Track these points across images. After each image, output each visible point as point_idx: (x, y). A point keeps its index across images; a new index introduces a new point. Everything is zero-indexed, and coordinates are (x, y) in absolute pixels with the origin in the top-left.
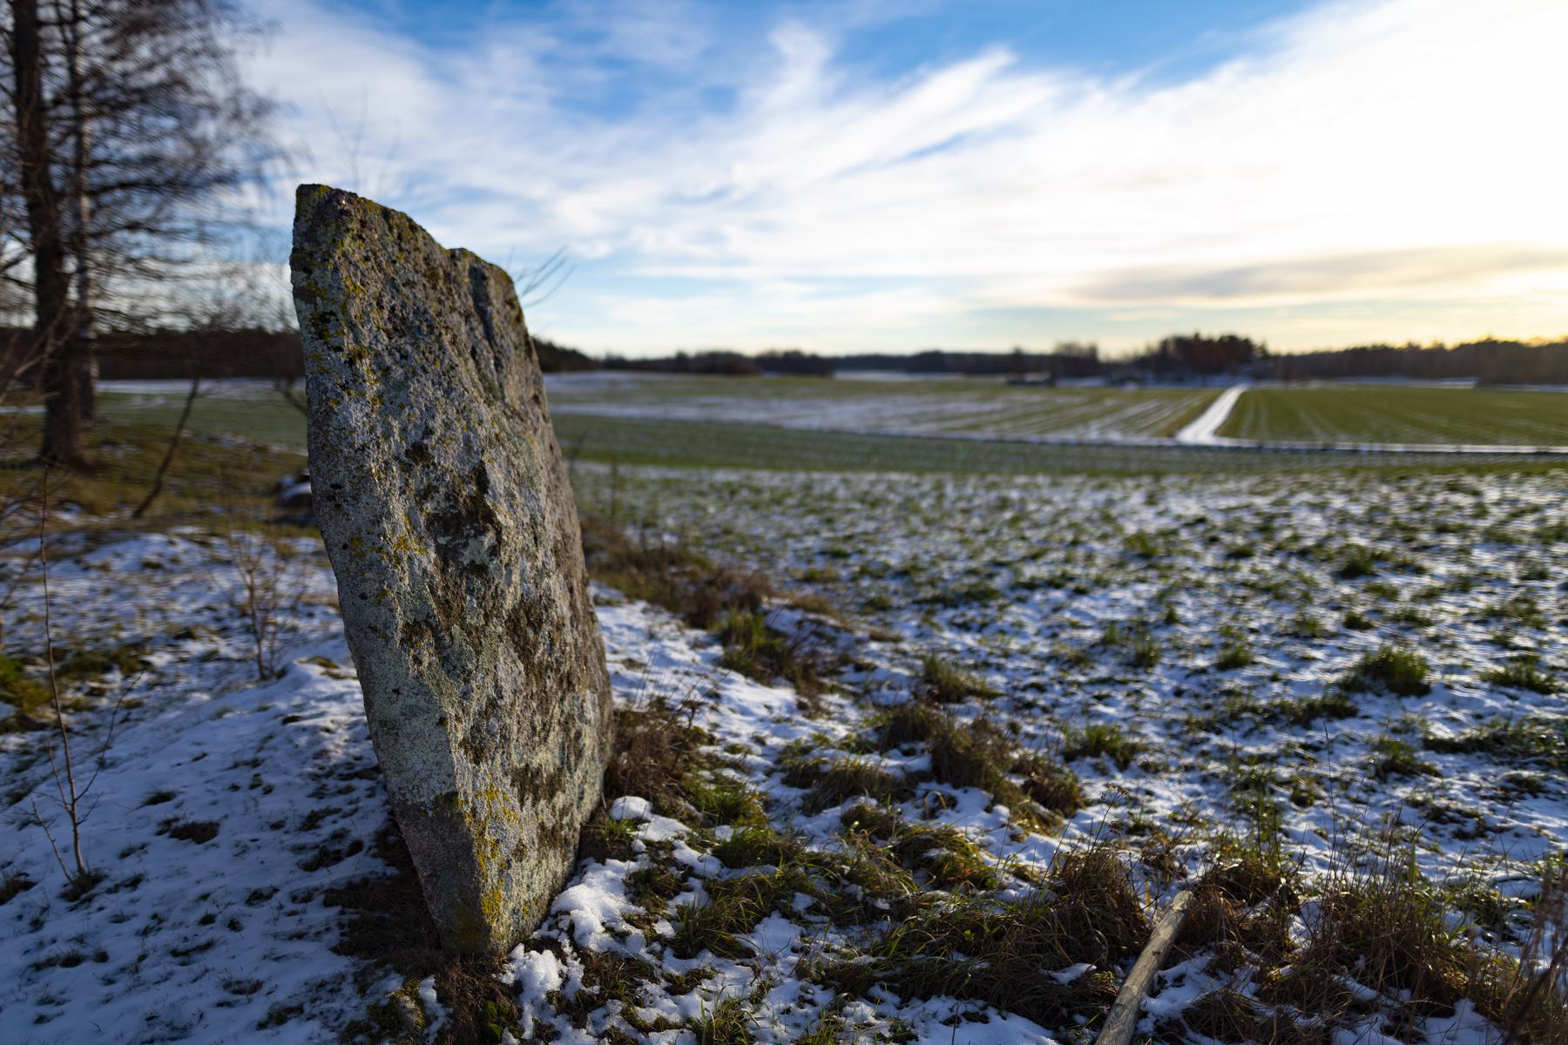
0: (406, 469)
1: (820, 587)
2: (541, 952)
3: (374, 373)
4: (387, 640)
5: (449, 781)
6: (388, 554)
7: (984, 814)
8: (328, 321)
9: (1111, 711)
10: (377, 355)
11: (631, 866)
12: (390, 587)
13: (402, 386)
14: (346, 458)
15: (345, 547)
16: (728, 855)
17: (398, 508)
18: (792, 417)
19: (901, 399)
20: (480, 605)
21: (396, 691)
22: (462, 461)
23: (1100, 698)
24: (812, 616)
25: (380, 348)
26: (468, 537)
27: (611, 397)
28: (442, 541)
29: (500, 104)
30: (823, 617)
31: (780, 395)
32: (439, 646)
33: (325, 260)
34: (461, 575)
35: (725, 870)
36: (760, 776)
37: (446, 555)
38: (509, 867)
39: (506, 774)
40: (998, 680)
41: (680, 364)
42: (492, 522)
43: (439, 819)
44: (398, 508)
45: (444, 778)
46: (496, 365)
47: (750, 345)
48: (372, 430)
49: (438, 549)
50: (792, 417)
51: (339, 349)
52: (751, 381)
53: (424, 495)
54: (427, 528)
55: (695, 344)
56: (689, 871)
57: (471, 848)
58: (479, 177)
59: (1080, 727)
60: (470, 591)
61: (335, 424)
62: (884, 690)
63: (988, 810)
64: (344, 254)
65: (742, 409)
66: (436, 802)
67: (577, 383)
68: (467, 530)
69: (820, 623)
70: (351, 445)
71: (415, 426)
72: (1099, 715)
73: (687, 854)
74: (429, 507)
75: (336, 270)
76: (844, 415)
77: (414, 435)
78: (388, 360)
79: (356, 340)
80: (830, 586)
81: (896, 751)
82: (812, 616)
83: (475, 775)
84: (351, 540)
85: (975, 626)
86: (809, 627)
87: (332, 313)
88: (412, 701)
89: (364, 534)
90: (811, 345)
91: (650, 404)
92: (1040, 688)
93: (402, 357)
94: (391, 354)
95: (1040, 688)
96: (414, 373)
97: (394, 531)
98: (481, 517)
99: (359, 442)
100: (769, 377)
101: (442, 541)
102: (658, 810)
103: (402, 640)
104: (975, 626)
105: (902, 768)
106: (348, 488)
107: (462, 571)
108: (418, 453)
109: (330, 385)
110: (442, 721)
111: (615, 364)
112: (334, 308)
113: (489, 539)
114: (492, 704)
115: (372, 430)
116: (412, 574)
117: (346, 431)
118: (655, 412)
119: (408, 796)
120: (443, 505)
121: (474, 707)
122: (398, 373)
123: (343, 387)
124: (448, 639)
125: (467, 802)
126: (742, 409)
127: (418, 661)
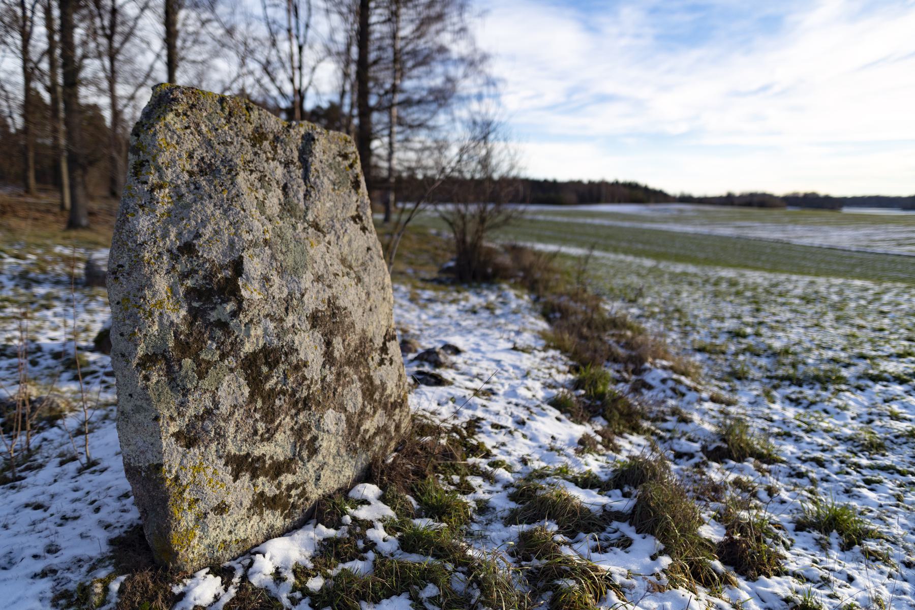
0: (174, 257)
1: (707, 355)
2: (215, 576)
3: (171, 197)
4: (128, 362)
5: (158, 456)
6: (144, 310)
7: (648, 560)
8: (144, 165)
9: (872, 495)
10: (177, 186)
11: (331, 532)
12: (140, 330)
13: (188, 206)
14: (129, 250)
15: (118, 303)
16: (410, 543)
17: (162, 284)
18: (802, 237)
19: (891, 227)
20: (218, 348)
21: (131, 395)
22: (225, 255)
23: (868, 482)
24: (675, 376)
25: (179, 182)
26: (216, 304)
27: (677, 220)
28: (196, 304)
29: (624, 42)
30: (683, 378)
31: (795, 222)
32: (169, 371)
33: (149, 128)
34: (206, 327)
35: (400, 551)
36: (499, 487)
37: (194, 314)
38: (206, 517)
39: (220, 457)
40: (789, 448)
41: (729, 200)
42: (235, 295)
43: (148, 479)
44: (162, 284)
45: (156, 454)
46: (305, 195)
47: (780, 189)
48: (154, 232)
49: (191, 310)
50: (802, 237)
51: (146, 183)
52: (776, 212)
53: (184, 276)
54: (185, 296)
55: (739, 189)
56: (371, 545)
57: (167, 501)
58: (609, 87)
59: (831, 500)
60: (212, 338)
61: (127, 228)
62: (683, 440)
63: (653, 558)
64: (166, 125)
65: (765, 230)
66: (148, 468)
67: (658, 210)
68: (216, 299)
69: (679, 382)
70: (135, 242)
71: (189, 231)
72: (859, 497)
73: (378, 534)
74: (189, 283)
75: (155, 134)
76: (841, 236)
77: (186, 237)
78: (183, 190)
79: (161, 177)
80: (714, 357)
81: (618, 492)
82: (675, 376)
83: (184, 456)
84: (123, 299)
85: (805, 402)
86: (671, 384)
87: (147, 161)
88: (139, 403)
89: (131, 296)
90: (823, 190)
91: (702, 225)
92: (820, 463)
93: (197, 188)
94: (188, 186)
95: (820, 463)
96: (202, 199)
97: (154, 296)
98: (230, 289)
99: (140, 239)
100: (790, 210)
101: (196, 304)
102: (383, 499)
103: (138, 364)
104: (805, 402)
105: (604, 506)
106: (127, 267)
107: (209, 325)
108: (188, 249)
109: (132, 205)
110: (157, 419)
111: (686, 199)
112: (148, 157)
113: (230, 307)
114: (209, 412)
115: (154, 232)
116: (161, 324)
117: (133, 233)
118: (704, 230)
119: (132, 460)
120: (201, 282)
121: (191, 412)
122: (189, 198)
123: (141, 206)
124: (177, 368)
125: (170, 472)
126: (765, 230)
127: (147, 378)
